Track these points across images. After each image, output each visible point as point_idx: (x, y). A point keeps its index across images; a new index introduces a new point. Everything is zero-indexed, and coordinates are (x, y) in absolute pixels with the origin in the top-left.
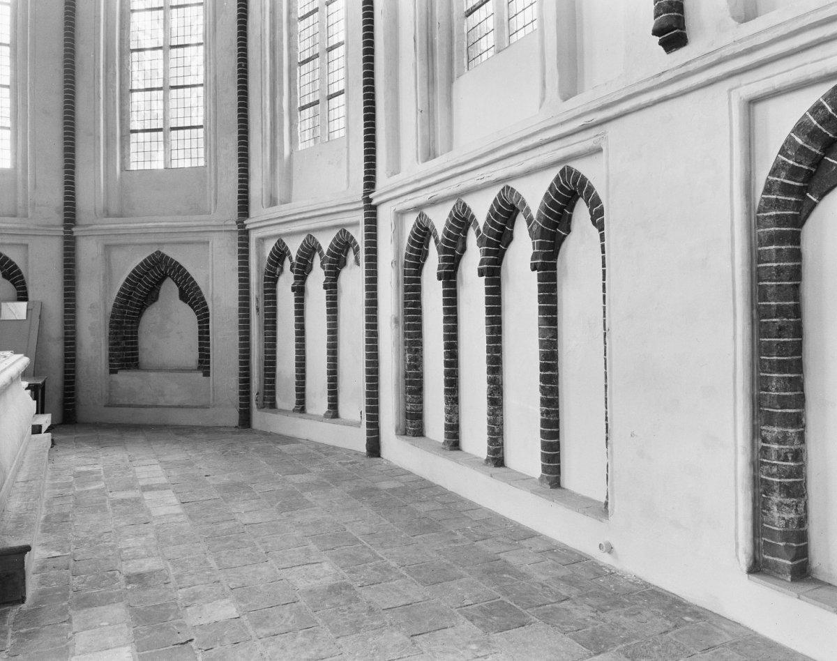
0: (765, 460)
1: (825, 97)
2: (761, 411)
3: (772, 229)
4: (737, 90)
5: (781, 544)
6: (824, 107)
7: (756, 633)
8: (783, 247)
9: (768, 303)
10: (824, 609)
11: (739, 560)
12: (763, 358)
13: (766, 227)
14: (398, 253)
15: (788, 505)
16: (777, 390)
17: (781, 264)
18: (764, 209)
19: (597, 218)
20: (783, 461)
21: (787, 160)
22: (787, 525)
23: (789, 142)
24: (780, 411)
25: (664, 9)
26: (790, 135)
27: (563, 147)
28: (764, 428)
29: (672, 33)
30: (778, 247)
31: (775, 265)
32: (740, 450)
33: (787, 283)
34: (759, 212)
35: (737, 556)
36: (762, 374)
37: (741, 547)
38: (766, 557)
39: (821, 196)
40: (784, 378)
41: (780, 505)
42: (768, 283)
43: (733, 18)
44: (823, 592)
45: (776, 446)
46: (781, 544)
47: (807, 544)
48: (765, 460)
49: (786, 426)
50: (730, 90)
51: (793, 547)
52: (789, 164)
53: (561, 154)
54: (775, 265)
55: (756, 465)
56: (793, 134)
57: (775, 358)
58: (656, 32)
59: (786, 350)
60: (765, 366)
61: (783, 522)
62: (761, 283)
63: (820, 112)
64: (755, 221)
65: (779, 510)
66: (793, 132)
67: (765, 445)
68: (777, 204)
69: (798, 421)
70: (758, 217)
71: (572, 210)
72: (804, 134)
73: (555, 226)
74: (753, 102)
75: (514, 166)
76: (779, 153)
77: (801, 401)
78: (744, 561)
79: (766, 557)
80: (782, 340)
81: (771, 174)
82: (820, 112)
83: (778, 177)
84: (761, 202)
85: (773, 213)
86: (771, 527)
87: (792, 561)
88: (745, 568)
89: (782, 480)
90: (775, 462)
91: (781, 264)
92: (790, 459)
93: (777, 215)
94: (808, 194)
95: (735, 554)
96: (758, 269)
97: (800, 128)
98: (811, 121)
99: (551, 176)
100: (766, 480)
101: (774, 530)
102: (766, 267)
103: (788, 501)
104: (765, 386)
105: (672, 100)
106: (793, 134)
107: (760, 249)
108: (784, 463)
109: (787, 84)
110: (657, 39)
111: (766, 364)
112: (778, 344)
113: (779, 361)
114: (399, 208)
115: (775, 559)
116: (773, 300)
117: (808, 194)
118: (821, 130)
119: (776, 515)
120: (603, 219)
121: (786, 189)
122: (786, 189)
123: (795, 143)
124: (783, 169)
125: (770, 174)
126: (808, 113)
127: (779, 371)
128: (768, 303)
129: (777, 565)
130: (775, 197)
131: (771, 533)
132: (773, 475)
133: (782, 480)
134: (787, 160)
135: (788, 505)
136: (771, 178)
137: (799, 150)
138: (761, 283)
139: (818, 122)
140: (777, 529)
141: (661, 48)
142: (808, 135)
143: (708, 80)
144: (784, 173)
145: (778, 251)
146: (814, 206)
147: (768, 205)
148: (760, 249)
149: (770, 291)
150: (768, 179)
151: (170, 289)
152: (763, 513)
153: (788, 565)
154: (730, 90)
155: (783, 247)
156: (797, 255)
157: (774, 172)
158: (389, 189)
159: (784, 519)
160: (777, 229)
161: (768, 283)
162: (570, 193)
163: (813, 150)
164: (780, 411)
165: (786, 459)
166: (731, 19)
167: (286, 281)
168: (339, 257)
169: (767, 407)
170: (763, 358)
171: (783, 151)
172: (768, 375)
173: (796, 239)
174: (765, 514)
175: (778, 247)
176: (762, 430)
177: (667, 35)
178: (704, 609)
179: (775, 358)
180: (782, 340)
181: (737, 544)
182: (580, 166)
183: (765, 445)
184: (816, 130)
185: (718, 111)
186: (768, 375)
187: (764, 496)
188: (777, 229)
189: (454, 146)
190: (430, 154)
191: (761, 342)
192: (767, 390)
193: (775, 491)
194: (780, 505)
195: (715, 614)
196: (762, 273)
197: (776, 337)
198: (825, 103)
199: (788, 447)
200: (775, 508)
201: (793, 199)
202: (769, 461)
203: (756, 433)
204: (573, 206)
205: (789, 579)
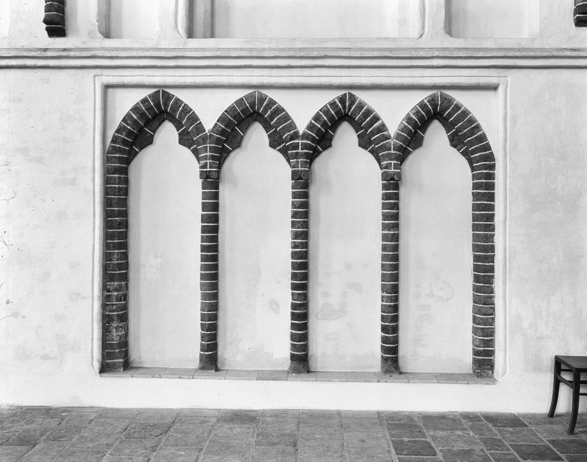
0: (108, 303)
1: (150, 96)
2: (106, 274)
3: (116, 165)
4: (100, 77)
5: (117, 351)
6: (148, 101)
7: (105, 408)
8: (122, 176)
9: (113, 209)
10: (147, 377)
11: (93, 367)
12: (108, 241)
13: (112, 163)
15: (121, 327)
16: (117, 260)
17: (121, 186)
18: (112, 152)
20: (119, 301)
21: (126, 126)
22: (120, 339)
23: (128, 116)
24: (118, 272)
25: (55, 9)
26: (129, 112)
27: (505, 140)
28: (108, 283)
29: (56, 26)
30: (119, 176)
31: (117, 186)
32: (96, 299)
33: (123, 197)
34: (108, 154)
35: (92, 365)
36: (107, 251)
37: (95, 359)
38: (108, 361)
39: (141, 148)
40: (120, 253)
41: (116, 328)
42: (113, 197)
43: (100, 32)
44: (140, 371)
45: (116, 293)
46: (117, 351)
47: (217, 282)
48: (108, 303)
49: (121, 281)
50: (95, 76)
51: (123, 351)
52: (128, 129)
54: (117, 186)
55: (104, 306)
56: (130, 112)
57: (116, 241)
58: (45, 21)
59: (122, 236)
60: (110, 246)
61: (118, 338)
62: (108, 197)
63: (147, 103)
64: (107, 159)
65: (117, 331)
66: (130, 110)
67: (108, 294)
68: (119, 150)
69: (125, 277)
70: (107, 157)
71: (245, 130)
72: (137, 113)
74: (107, 87)
76: (122, 121)
77: (126, 266)
78: (97, 366)
79: (108, 361)
80: (120, 230)
81: (116, 132)
82: (147, 103)
83: (121, 135)
84: (109, 147)
85: (117, 155)
86: (112, 342)
87: (123, 359)
88: (98, 371)
89: (118, 313)
90: (115, 303)
91: (121, 186)
93: (119, 157)
94: (134, 147)
95: (91, 364)
96: (107, 187)
97: (135, 109)
98: (141, 107)
100: (109, 315)
101: (113, 344)
102: (111, 187)
103: (121, 324)
104: (109, 259)
105: (50, 70)
106: (130, 112)
107: (108, 176)
108: (120, 303)
109: (132, 83)
110: (45, 26)
111: (111, 245)
112: (119, 232)
113: (119, 243)
115: (113, 361)
116: (115, 207)
117: (134, 147)
118: (146, 113)
119: (115, 334)
121: (125, 143)
122: (125, 143)
123: (132, 117)
124: (124, 130)
125: (116, 132)
126: (140, 102)
127: (118, 249)
128: (113, 209)
129: (114, 364)
130: (118, 146)
131: (111, 346)
132: (113, 311)
133: (118, 313)
134: (126, 126)
135: (121, 327)
136: (116, 134)
137: (134, 122)
138: (108, 197)
139: (145, 109)
140: (115, 342)
142: (140, 114)
143: (82, 66)
144: (124, 133)
145: (119, 178)
146: (137, 153)
147: (114, 150)
148: (108, 176)
149: (114, 201)
150: (114, 134)
152: (106, 335)
153: (121, 362)
154: (95, 76)
155: (122, 176)
156: (126, 181)
157: (118, 131)
159: (119, 335)
160: (119, 165)
161: (113, 197)
163: (141, 123)
164: (118, 272)
165: (120, 300)
166: (98, 32)
168: (141, 130)
169: (110, 271)
170: (108, 241)
171: (124, 120)
172: (112, 251)
173: (125, 171)
174: (108, 335)
175: (119, 176)
176: (107, 285)
177: (53, 26)
178: (68, 407)
179: (116, 241)
180: (120, 230)
181: (92, 357)
183: (108, 294)
184: (144, 113)
185: (89, 84)
186: (112, 251)
187: (107, 324)
188: (119, 165)
191: (107, 232)
192: (110, 260)
193: (114, 320)
194: (116, 328)
195: (77, 407)
196: (109, 190)
197: (117, 229)
198: (149, 99)
199: (122, 293)
200: (114, 330)
201: (127, 149)
202: (111, 303)
203: (105, 288)
205: (122, 370)
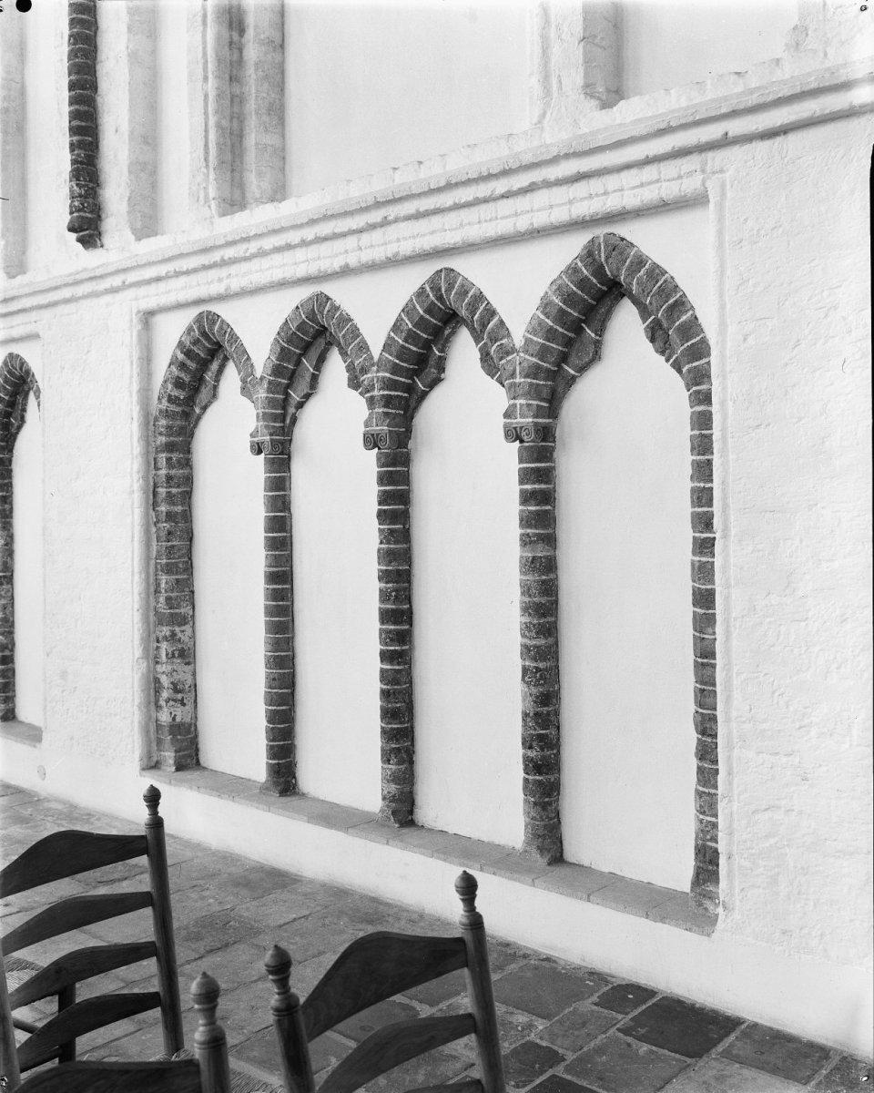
14: (145, 391)
19: (38, 397)
53: (202, 292)
58: (71, 229)
64: (148, 422)
73: (413, 374)
75: (239, 277)
88: (138, 768)
92: (177, 655)
99: (569, 250)
110: (74, 236)
114: (151, 303)
120: (709, 363)
141: (79, 245)
151: (626, 325)
158: (786, 92)
162: (599, 291)
167: (231, 419)
182: (226, 312)
185: (120, 313)
189: (294, 180)
190: (234, 201)
204: (448, 340)
